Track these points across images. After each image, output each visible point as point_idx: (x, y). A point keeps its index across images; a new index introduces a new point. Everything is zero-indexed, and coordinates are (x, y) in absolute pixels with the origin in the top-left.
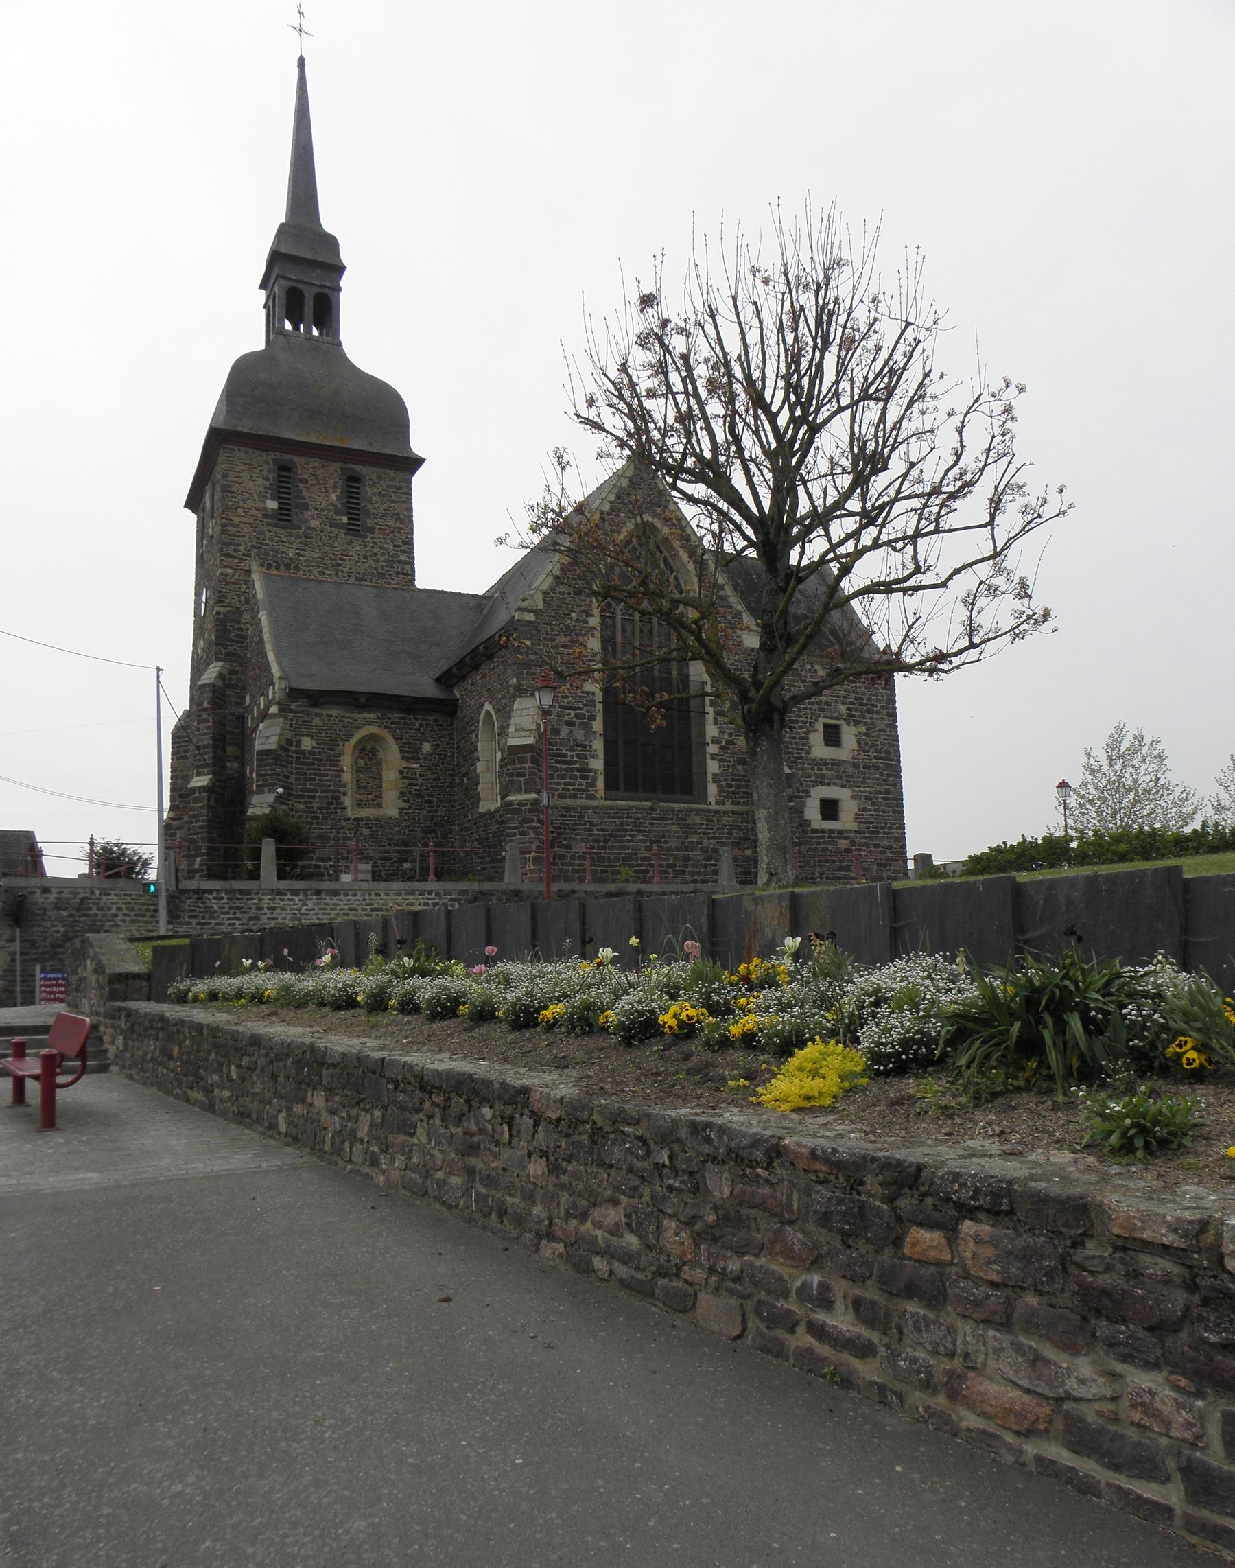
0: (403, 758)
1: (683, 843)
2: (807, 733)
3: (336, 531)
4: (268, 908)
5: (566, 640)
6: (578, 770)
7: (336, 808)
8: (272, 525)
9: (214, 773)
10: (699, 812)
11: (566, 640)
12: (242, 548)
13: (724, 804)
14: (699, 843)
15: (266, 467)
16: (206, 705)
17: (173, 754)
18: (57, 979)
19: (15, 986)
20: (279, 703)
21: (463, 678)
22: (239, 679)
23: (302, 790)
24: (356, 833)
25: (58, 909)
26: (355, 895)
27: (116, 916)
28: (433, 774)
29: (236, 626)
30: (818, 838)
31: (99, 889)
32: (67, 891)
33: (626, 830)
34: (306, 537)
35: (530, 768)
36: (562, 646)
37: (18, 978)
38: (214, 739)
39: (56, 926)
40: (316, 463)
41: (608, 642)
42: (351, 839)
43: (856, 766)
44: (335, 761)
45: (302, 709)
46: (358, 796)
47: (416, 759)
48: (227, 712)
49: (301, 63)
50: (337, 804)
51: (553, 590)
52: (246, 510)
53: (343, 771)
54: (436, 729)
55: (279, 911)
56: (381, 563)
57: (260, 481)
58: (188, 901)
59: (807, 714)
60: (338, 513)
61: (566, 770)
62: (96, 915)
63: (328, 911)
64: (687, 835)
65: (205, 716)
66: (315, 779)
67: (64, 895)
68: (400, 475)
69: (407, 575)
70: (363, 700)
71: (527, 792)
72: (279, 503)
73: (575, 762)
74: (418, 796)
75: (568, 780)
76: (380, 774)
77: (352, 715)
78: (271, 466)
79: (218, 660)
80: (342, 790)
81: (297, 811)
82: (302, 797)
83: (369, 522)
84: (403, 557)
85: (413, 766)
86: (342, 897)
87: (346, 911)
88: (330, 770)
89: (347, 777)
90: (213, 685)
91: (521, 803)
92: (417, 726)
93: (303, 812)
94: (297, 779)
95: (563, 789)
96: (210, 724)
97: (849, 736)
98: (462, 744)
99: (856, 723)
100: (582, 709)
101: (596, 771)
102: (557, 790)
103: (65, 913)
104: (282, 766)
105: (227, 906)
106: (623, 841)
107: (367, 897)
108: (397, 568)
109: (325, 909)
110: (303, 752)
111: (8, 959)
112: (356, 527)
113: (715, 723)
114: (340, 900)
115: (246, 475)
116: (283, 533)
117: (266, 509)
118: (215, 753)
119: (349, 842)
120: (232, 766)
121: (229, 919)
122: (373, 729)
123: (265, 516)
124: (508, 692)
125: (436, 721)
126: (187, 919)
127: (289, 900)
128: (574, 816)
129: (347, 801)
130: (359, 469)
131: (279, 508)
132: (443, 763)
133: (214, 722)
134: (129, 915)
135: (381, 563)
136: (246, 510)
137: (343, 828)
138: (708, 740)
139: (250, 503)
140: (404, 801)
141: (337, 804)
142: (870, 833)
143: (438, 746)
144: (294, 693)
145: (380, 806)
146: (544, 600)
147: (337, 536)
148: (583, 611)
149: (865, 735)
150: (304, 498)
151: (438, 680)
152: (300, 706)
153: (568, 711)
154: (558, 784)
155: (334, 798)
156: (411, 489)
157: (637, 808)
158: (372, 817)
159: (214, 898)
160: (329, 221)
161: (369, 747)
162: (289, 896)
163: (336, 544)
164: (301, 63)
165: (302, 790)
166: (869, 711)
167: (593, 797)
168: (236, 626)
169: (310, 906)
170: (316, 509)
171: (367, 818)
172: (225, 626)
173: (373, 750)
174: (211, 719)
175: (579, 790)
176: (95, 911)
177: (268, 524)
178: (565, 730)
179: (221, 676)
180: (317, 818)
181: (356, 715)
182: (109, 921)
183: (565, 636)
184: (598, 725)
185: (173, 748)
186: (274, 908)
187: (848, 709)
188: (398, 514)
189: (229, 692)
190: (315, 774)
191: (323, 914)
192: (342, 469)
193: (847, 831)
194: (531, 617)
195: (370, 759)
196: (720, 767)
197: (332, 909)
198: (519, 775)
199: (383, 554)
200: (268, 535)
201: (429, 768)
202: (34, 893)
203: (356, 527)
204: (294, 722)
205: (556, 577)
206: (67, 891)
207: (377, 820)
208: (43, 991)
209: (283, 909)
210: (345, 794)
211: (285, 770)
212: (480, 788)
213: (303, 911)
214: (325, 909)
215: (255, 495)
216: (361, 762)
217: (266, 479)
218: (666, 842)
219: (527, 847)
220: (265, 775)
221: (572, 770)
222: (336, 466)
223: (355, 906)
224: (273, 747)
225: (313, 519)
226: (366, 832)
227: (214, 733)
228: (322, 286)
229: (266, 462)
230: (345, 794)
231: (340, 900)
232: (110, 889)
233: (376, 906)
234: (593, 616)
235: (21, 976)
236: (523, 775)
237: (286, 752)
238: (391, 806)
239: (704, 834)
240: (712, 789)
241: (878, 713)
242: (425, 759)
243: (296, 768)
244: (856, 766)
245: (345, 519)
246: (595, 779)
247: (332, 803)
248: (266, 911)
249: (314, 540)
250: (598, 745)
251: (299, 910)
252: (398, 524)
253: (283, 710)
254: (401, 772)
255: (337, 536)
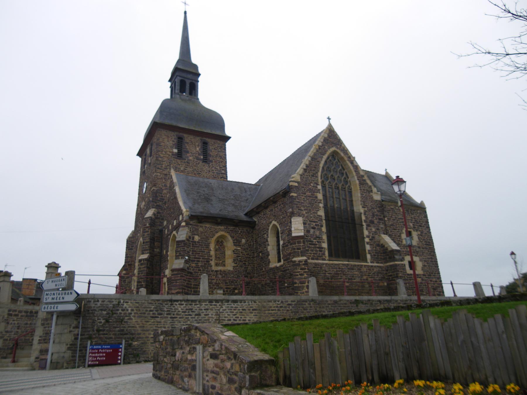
0: (234, 245)
1: (361, 280)
2: (400, 234)
3: (199, 161)
4: (205, 309)
5: (310, 194)
6: (318, 248)
7: (208, 266)
8: (175, 158)
9: (150, 253)
10: (365, 266)
11: (310, 194)
12: (164, 166)
13: (373, 263)
14: (367, 279)
15: (173, 137)
16: (148, 225)
17: (127, 248)
18: (98, 349)
19: (76, 353)
20: (185, 221)
21: (258, 213)
22: (161, 216)
23: (194, 258)
24: (216, 277)
25: (102, 310)
26: (245, 302)
27: (131, 314)
28: (246, 252)
29: (160, 195)
30: (410, 277)
31: (123, 299)
32: (106, 301)
33: (339, 274)
34: (188, 163)
35: (303, 246)
36: (309, 197)
37: (78, 349)
38: (151, 239)
39: (100, 319)
40: (192, 137)
41: (325, 196)
42: (214, 279)
43: (419, 248)
44: (208, 246)
45: (194, 224)
46: (216, 261)
47: (240, 246)
48: (156, 228)
49: (185, 13)
50: (208, 264)
51: (304, 174)
52: (166, 152)
53: (211, 250)
54: (247, 233)
55: (209, 311)
56: (215, 174)
57: (171, 142)
58: (166, 306)
59: (399, 226)
60: (199, 155)
61: (314, 248)
62: (121, 313)
63: (233, 311)
64: (362, 276)
65: (147, 230)
66: (199, 254)
67: (105, 303)
68: (222, 143)
69: (225, 178)
70: (219, 220)
71: (302, 256)
72: (178, 150)
73: (317, 245)
74: (241, 261)
75: (314, 252)
76: (224, 252)
77: (214, 227)
78: (176, 137)
79: (153, 208)
80: (211, 258)
81: (192, 267)
82: (195, 261)
83: (211, 159)
84: (223, 172)
85: (239, 249)
86: (239, 303)
87: (241, 311)
88: (205, 250)
89: (212, 253)
90: (151, 217)
91: (300, 261)
92: (240, 232)
93: (195, 267)
94: (192, 253)
95: (313, 256)
96: (149, 233)
97: (415, 234)
98: (259, 240)
99: (417, 231)
100: (317, 222)
101: (325, 248)
102: (310, 256)
103: (105, 313)
104: (187, 247)
105: (185, 308)
106: (338, 279)
107: (250, 303)
108: (221, 175)
109: (231, 310)
110: (195, 242)
111: (73, 338)
112: (206, 160)
113: (367, 229)
114: (238, 305)
115: (166, 140)
116: (179, 161)
117: (173, 152)
118: (151, 245)
119: (213, 281)
120: (157, 250)
121: (186, 315)
122: (220, 233)
123: (173, 155)
124: (287, 215)
125: (247, 230)
126: (165, 315)
127: (215, 305)
128: (318, 268)
129: (213, 263)
130: (208, 140)
131: (178, 152)
132: (250, 248)
133: (151, 232)
134: (137, 313)
135: (215, 174)
136: (166, 152)
137: (211, 275)
138: (365, 236)
139: (167, 150)
140: (235, 263)
141: (208, 264)
142: (428, 275)
143: (248, 240)
144: (192, 217)
145: (224, 265)
146: (301, 178)
147: (199, 163)
148: (315, 183)
149: (420, 235)
150: (187, 149)
151: (246, 215)
152: (194, 223)
153: (312, 223)
154: (311, 253)
155: (207, 262)
156: (226, 148)
157: (343, 264)
158: (222, 270)
159: (179, 304)
160: (194, 59)
161: (220, 240)
162: (214, 303)
163: (199, 166)
164: (185, 13)
165: (194, 258)
166: (420, 226)
167: (324, 260)
168: (160, 195)
169: (224, 308)
170: (192, 153)
171: (221, 271)
172: (156, 195)
173: (222, 242)
174: (149, 231)
175: (319, 256)
176: (120, 311)
177: (173, 158)
178: (312, 231)
179: (154, 214)
180: (200, 270)
181: (216, 227)
182: (126, 316)
183: (310, 192)
184: (324, 229)
185: (127, 245)
186: (207, 309)
187: (413, 225)
188: (221, 156)
189: (156, 220)
190: (199, 251)
191: (230, 312)
192: (201, 139)
193: (420, 275)
194: (296, 184)
195: (221, 246)
196: (370, 247)
197: (234, 310)
198: (298, 249)
199: (216, 171)
200: (173, 161)
201: (244, 250)
202: (90, 302)
203: (206, 160)
204: (192, 229)
205: (304, 169)
206: (106, 301)
207: (224, 271)
208: (91, 356)
209: (212, 310)
210: (211, 260)
211: (188, 249)
212: (270, 257)
213: (221, 311)
214: (231, 310)
215: (169, 147)
216: (217, 247)
217: (173, 141)
218: (354, 279)
219: (304, 281)
220: (180, 251)
221: (316, 247)
222: (198, 138)
223: (245, 308)
224: (184, 239)
225: (190, 156)
226: (220, 276)
227: (151, 237)
228: (192, 80)
229: (174, 136)
230: (211, 260)
231: (238, 305)
232: (129, 300)
233: (255, 308)
234: (319, 185)
235: (80, 347)
236: (300, 249)
237: (188, 242)
238: (229, 265)
239: (368, 275)
240: (369, 256)
241: (424, 227)
242: (243, 246)
243: (192, 249)
244: (419, 248)
245: (202, 157)
246: (325, 252)
247: (206, 264)
248: (203, 311)
249: (190, 164)
250: (325, 237)
251: (219, 310)
252: (221, 160)
253: (187, 224)
254: (234, 251)
255: (199, 163)
